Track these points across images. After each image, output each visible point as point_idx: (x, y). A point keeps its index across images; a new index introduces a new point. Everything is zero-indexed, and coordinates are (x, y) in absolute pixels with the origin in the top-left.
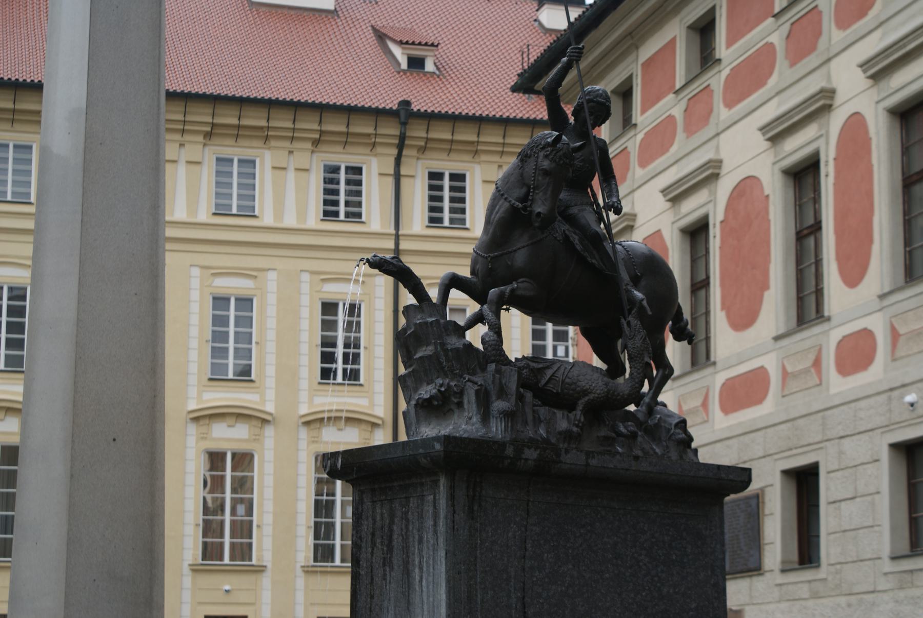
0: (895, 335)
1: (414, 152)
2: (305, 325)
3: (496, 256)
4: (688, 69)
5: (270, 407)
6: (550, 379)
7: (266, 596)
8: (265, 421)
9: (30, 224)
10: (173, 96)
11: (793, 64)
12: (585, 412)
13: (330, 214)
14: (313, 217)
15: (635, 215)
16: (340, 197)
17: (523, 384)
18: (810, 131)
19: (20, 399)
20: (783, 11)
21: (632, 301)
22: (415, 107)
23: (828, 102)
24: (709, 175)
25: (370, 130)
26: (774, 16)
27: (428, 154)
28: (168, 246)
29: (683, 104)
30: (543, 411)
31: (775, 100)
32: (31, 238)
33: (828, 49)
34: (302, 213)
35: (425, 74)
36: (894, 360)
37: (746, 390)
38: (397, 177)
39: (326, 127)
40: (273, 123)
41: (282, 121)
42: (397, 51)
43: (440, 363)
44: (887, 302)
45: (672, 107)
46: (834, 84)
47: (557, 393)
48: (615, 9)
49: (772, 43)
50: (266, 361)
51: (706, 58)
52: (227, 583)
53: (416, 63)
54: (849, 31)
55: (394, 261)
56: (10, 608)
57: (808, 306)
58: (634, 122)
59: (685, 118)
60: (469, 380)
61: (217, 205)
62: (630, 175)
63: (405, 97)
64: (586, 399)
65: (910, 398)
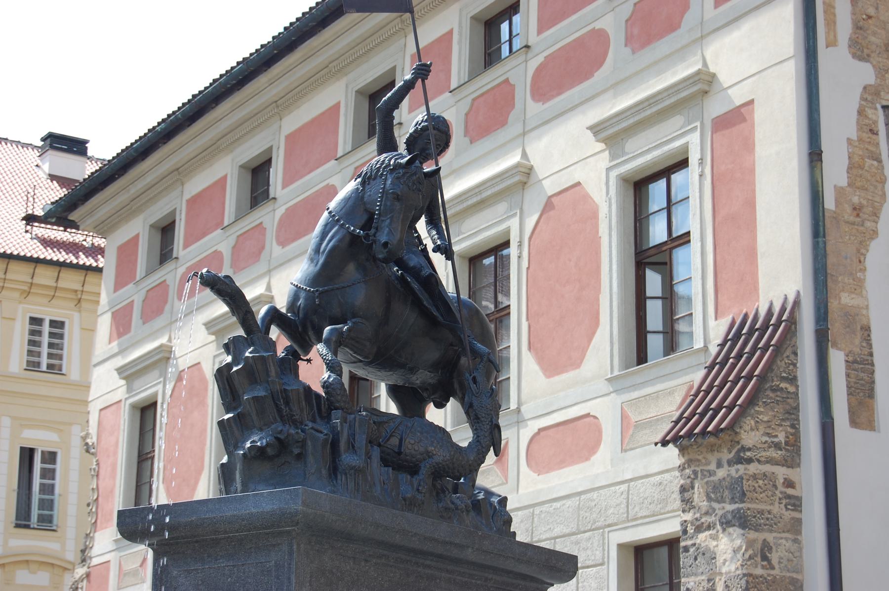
4: (238, 208)
23: (706, 88)
24: (522, 178)
29: (232, 240)
36: (623, 450)
37: (573, 439)
46: (712, 69)
48: (143, 160)
49: (333, 185)
54: (547, 105)
58: (272, 195)
59: (233, 254)
60: (312, 428)
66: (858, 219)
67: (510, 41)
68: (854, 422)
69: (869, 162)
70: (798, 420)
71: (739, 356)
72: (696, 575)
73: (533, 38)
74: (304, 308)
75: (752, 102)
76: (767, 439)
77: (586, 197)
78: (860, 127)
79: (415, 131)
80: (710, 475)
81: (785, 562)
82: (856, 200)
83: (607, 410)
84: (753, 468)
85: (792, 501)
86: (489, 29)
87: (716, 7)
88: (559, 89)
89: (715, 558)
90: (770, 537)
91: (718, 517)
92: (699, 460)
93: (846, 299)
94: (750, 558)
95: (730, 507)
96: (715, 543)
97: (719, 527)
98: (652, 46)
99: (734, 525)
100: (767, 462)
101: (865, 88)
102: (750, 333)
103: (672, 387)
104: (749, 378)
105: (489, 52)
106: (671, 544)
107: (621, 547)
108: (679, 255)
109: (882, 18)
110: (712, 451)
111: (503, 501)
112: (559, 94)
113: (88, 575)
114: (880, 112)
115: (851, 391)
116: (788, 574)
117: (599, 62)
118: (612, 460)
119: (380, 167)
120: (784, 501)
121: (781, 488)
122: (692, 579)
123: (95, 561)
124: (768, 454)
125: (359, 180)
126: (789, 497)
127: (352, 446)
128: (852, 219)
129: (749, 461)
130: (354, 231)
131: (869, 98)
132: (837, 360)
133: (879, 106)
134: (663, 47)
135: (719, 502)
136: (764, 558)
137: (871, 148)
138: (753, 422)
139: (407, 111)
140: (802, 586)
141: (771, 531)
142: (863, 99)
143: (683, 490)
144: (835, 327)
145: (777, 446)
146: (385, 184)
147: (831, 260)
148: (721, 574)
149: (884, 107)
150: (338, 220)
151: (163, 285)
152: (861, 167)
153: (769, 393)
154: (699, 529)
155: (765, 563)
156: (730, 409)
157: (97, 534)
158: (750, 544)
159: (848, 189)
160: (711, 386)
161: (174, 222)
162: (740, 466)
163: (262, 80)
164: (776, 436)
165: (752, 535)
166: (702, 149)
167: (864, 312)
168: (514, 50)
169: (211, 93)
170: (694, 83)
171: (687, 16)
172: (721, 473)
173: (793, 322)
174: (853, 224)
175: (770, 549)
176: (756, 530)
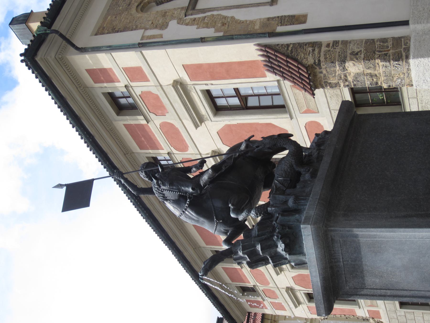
3: (216, 216)
6: (282, 184)
36: (318, 112)
43: (266, 239)
46: (172, 82)
47: (291, 180)
48: (217, 298)
51: (252, 290)
54: (189, 146)
55: (206, 263)
60: (276, 221)
62: (272, 289)
64: (294, 166)
66: (227, 24)
67: (167, 160)
68: (304, 22)
69: (206, 21)
70: (303, 43)
71: (280, 67)
72: (365, 81)
74: (225, 227)
75: (183, 65)
76: (311, 55)
77: (223, 129)
78: (192, 24)
79: (147, 177)
80: (325, 76)
81: (359, 46)
82: (219, 25)
85: (335, 44)
87: (149, 81)
88: (183, 141)
89: (358, 73)
90: (349, 52)
91: (342, 73)
92: (320, 81)
93: (257, 27)
94: (357, 59)
96: (352, 74)
97: (346, 72)
98: (165, 105)
99: (345, 66)
100: (320, 54)
101: (178, 23)
102: (271, 63)
103: (292, 93)
104: (288, 62)
107: (401, 308)
108: (243, 92)
109: (153, 19)
110: (316, 75)
111: (317, 135)
112: (185, 141)
113: (373, 318)
114: (187, 17)
115: (292, 24)
116: (363, 44)
117: (172, 125)
118: (322, 117)
119: (159, 192)
120: (335, 47)
121: (330, 49)
122: (366, 82)
123: (368, 315)
124: (316, 54)
125: (165, 202)
126: (333, 45)
127: (286, 202)
128: (227, 26)
129: (319, 61)
130: (187, 204)
131: (182, 22)
132: (280, 29)
133: (185, 18)
134: (165, 100)
135: (336, 72)
136: (357, 54)
137: (200, 20)
138: (304, 60)
140: (368, 40)
141: (347, 52)
142: (182, 24)
143: (331, 87)
144: (268, 30)
145: (314, 50)
146: (166, 190)
149: (186, 16)
150: (183, 212)
152: (208, 24)
153: (293, 54)
154: (346, 80)
155: (359, 54)
156: (299, 68)
157: (358, 315)
158: (352, 60)
159: (216, 28)
160: (291, 77)
161: (241, 287)
162: (322, 64)
163: (185, 254)
164: (310, 51)
165: (348, 58)
167: (262, 20)
168: (170, 159)
169: (191, 273)
170: (178, 88)
171: (153, 92)
173: (266, 46)
174: (228, 26)
175: (354, 52)
176: (346, 57)
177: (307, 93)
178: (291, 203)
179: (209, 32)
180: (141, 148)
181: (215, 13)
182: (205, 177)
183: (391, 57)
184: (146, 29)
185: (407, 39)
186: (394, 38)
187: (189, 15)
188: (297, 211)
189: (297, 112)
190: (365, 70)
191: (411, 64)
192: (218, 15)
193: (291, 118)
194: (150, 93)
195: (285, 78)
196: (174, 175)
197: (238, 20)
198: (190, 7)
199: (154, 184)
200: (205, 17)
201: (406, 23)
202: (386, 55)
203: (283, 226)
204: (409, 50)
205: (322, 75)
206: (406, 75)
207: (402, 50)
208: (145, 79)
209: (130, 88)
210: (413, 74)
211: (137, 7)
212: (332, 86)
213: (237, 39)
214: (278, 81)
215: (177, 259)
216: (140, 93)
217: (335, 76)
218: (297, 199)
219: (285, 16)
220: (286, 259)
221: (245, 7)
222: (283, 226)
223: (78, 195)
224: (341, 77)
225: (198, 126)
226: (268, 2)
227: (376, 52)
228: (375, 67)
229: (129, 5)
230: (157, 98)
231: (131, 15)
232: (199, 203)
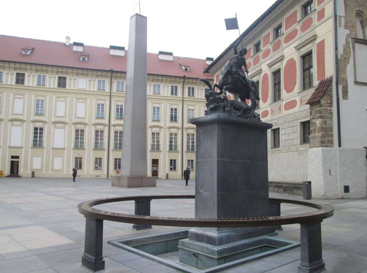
0: (272, 111)
1: (186, 84)
2: (168, 112)
5: (162, 125)
6: (236, 105)
7: (162, 156)
8: (86, 125)
9: (124, 95)
10: (149, 74)
11: (254, 66)
12: (243, 111)
13: (172, 94)
14: (169, 95)
15: (317, 35)
16: (174, 91)
17: (231, 105)
18: (257, 77)
19: (123, 124)
20: (252, 57)
21: (252, 90)
22: (186, 76)
24: (282, 58)
25: (179, 80)
26: (251, 57)
27: (188, 84)
28: (148, 99)
30: (235, 111)
31: (270, 59)
32: (124, 97)
33: (261, 63)
34: (167, 94)
35: (188, 71)
36: (301, 106)
38: (183, 88)
39: (37, 68)
40: (163, 79)
41: (164, 78)
42: (183, 67)
44: (271, 105)
45: (270, 47)
50: (162, 119)
52: (156, 153)
53: (186, 69)
56: (122, 157)
57: (277, 97)
61: (154, 92)
63: (185, 75)
64: (243, 109)
65: (275, 122)
67: (280, 33)
68: (344, 98)
69: (347, 49)
71: (321, 87)
72: (313, 127)
73: (284, 32)
76: (326, 102)
78: (346, 42)
83: (298, 99)
84: (323, 108)
86: (305, 7)
90: (327, 120)
93: (342, 75)
95: (319, 115)
103: (310, 93)
105: (305, 13)
106: (308, 122)
107: (301, 123)
114: (350, 39)
115: (343, 93)
117: (296, 35)
126: (330, 113)
128: (344, 60)
129: (323, 106)
132: (340, 87)
133: (350, 38)
134: (307, 31)
136: (325, 124)
139: (317, 5)
144: (340, 81)
145: (328, 103)
147: (340, 68)
148: (317, 127)
149: (351, 38)
151: (280, 41)
152: (346, 50)
153: (326, 94)
155: (325, 125)
161: (260, 43)
162: (321, 108)
165: (323, 120)
166: (315, 49)
167: (346, 78)
168: (311, 11)
172: (317, 109)
175: (326, 122)
176: (324, 119)
177: (308, 101)
178: (227, 109)
179: (341, 51)
180: (286, 19)
181: (352, 53)
182: (241, 74)
183: (323, 139)
184: (345, 18)
185: (332, 146)
186: (333, 140)
187: (352, 40)
188: (224, 111)
189: (301, 96)
190: (317, 127)
191: (319, 148)
192: (351, 55)
193: (298, 93)
194: (312, 23)
195: (316, 90)
196: (241, 63)
197: (347, 65)
198: (356, 40)
199: (237, 56)
200: (350, 49)
201: (340, 146)
202: (324, 137)
203: (219, 107)
204: (326, 147)
205: (316, 108)
206: (315, 146)
207: (326, 144)
208: (319, 20)
209: (314, 12)
210: (315, 149)
211: (359, 11)
212: (311, 112)
213: (336, 66)
214: (315, 87)
215: (259, 17)
216: (312, 17)
217: (315, 114)
218: (229, 111)
219: (348, 89)
220: (208, 108)
221: (354, 69)
222: (219, 107)
223: (232, 24)
224: (314, 116)
225: (295, 48)
226: (356, 80)
227: (326, 132)
228: (319, 132)
229: (361, 6)
230: (309, 26)
231: (355, 8)
232: (228, 73)
